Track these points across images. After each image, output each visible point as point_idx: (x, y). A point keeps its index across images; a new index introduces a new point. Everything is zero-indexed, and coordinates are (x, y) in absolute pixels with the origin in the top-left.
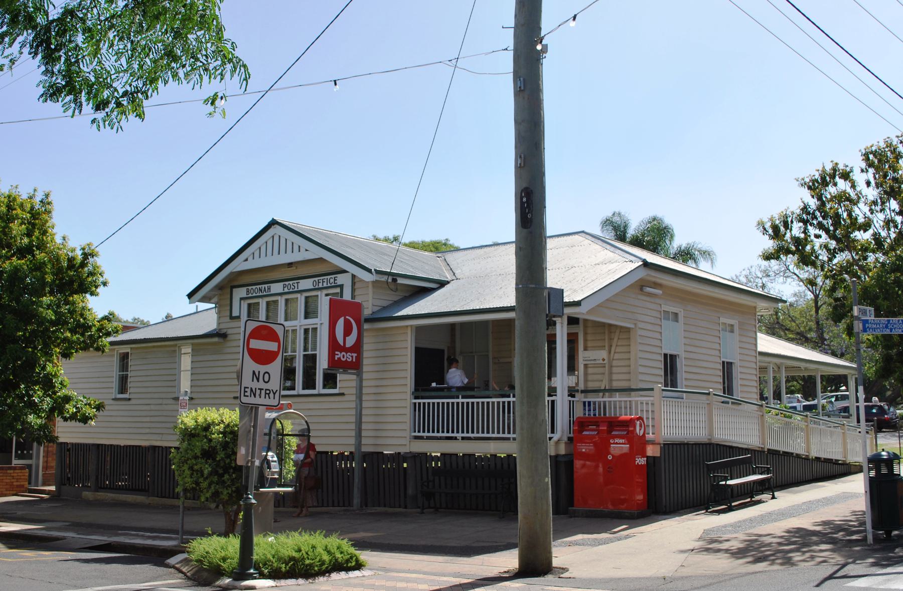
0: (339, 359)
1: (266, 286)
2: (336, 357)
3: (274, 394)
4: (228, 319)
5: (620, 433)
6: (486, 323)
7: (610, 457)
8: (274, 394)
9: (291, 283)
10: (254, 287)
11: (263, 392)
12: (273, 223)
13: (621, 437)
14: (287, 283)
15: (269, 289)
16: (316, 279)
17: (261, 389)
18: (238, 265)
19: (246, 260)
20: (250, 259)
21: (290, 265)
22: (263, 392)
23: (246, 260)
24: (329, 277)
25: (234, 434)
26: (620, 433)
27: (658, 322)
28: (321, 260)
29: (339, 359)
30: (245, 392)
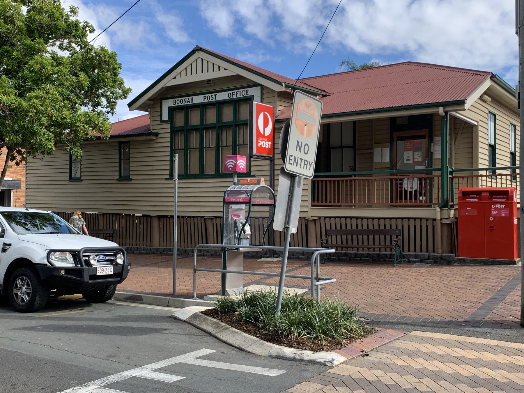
0: (261, 146)
1: (190, 98)
2: (259, 144)
3: (310, 165)
4: (159, 122)
5: (501, 200)
6: (371, 121)
7: (491, 219)
8: (310, 165)
9: (210, 95)
10: (180, 99)
11: (303, 161)
12: (198, 49)
13: (501, 203)
14: (207, 95)
15: (192, 100)
16: (231, 92)
17: (302, 160)
18: (169, 82)
19: (175, 78)
20: (178, 77)
21: (209, 81)
22: (303, 161)
23: (175, 78)
24: (241, 90)
25: (75, 112)
26: (501, 200)
27: (486, 120)
28: (238, 77)
29: (261, 146)
30: (290, 159)
